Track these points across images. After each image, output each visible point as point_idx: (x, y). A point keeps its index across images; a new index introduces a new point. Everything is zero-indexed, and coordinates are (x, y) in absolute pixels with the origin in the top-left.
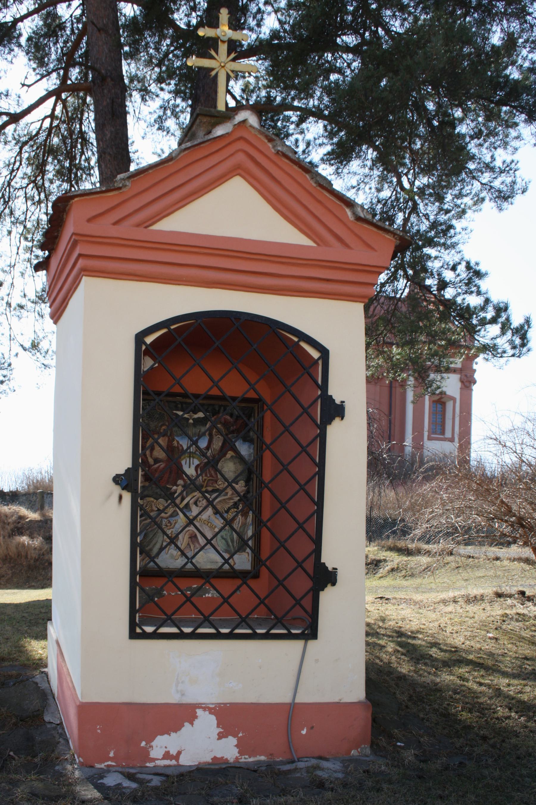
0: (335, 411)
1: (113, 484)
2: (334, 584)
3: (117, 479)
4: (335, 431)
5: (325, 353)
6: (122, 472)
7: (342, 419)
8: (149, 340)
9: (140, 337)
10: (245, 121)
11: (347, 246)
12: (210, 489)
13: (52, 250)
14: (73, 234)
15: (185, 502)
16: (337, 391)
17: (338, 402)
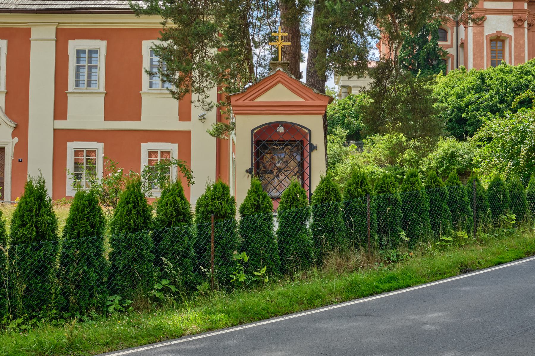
0: (313, 148)
3: (247, 171)
4: (314, 154)
5: (310, 131)
8: (255, 132)
9: (252, 131)
16: (314, 142)
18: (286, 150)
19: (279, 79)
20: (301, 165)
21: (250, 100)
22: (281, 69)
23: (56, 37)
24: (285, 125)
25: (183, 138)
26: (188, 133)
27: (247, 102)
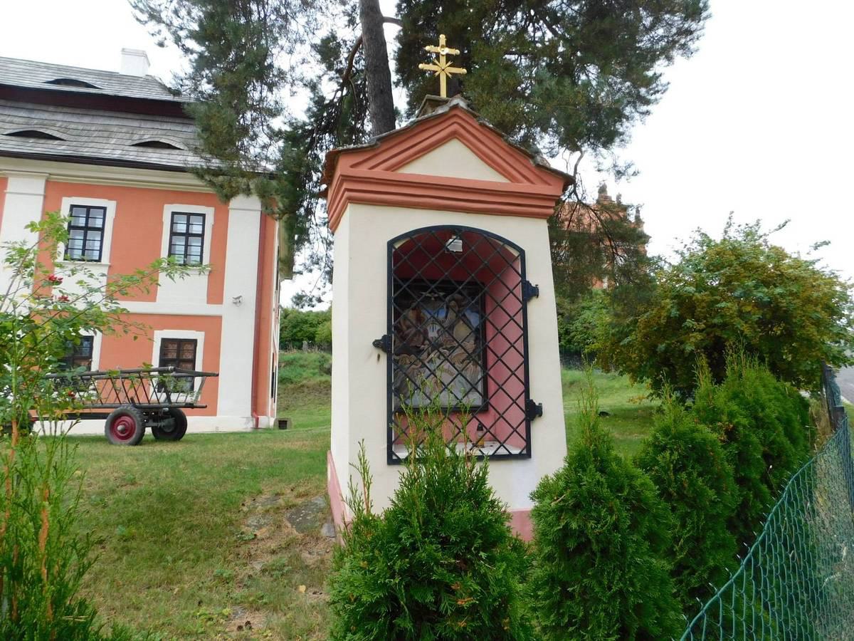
0: (531, 292)
1: (373, 347)
2: (541, 415)
3: (377, 344)
4: (533, 306)
5: (522, 252)
6: (380, 338)
7: (538, 296)
8: (397, 246)
9: (391, 244)
10: (458, 104)
11: (532, 183)
12: (449, 346)
13: (329, 184)
14: (341, 175)
15: (430, 357)
16: (532, 279)
17: (533, 285)
18: (450, 301)
19: (455, 127)
20: (480, 334)
21: (387, 169)
22: (462, 104)
23: (45, 191)
24: (466, 234)
25: (212, 325)
26: (219, 318)
27: (379, 173)
